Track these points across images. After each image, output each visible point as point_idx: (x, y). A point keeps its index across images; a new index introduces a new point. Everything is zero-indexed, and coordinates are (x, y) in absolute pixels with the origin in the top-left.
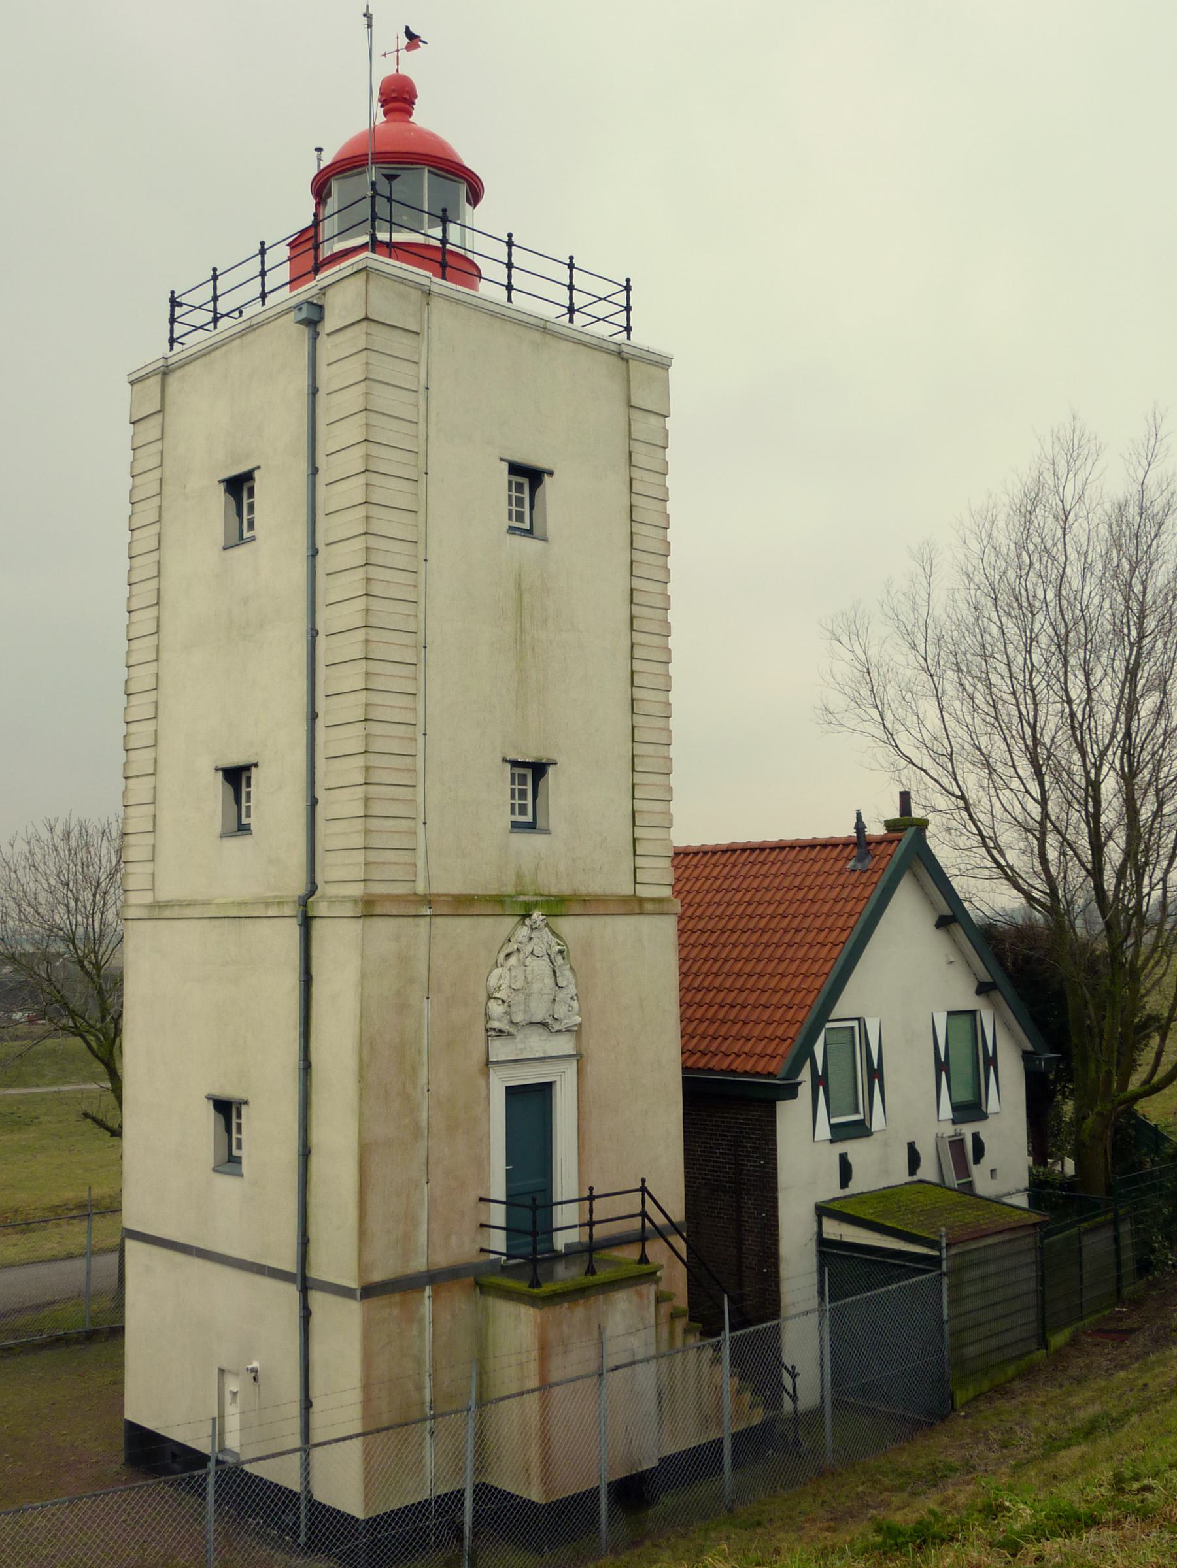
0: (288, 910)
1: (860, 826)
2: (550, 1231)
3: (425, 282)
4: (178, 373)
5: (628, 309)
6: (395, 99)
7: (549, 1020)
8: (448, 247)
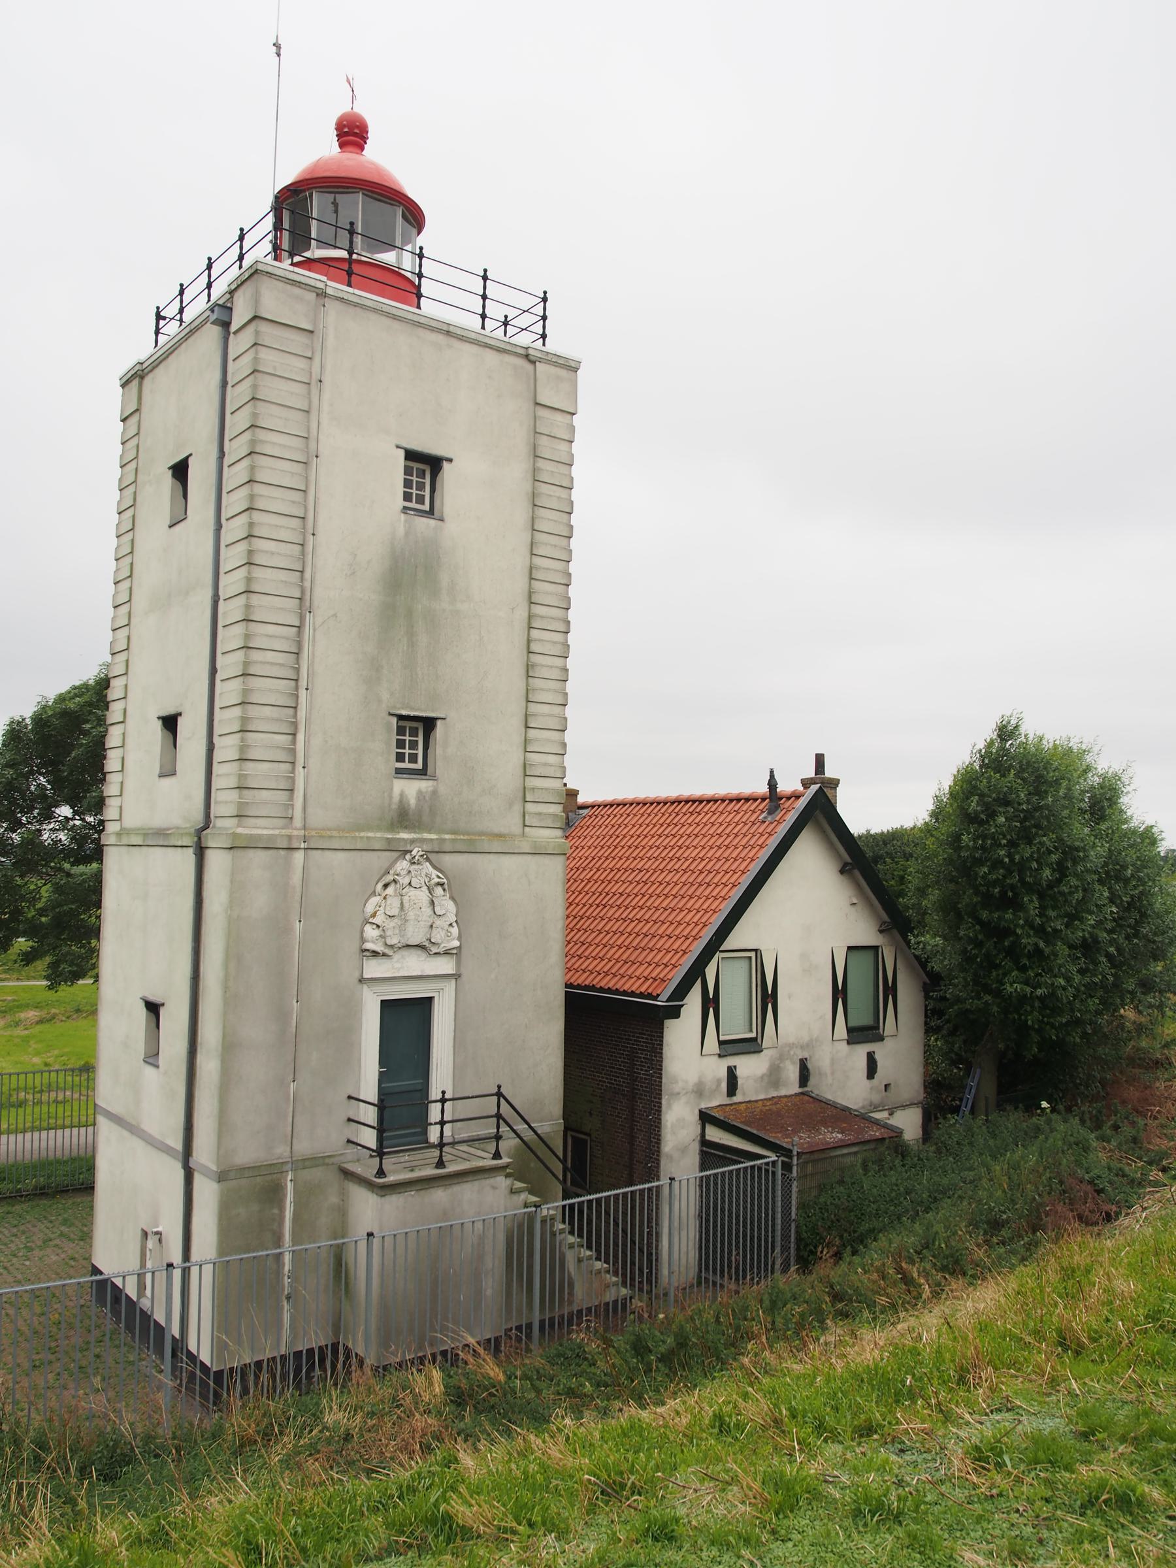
0: (188, 841)
1: (772, 784)
3: (321, 285)
4: (150, 376)
5: (544, 318)
6: (355, 135)
7: (427, 944)
8: (355, 256)
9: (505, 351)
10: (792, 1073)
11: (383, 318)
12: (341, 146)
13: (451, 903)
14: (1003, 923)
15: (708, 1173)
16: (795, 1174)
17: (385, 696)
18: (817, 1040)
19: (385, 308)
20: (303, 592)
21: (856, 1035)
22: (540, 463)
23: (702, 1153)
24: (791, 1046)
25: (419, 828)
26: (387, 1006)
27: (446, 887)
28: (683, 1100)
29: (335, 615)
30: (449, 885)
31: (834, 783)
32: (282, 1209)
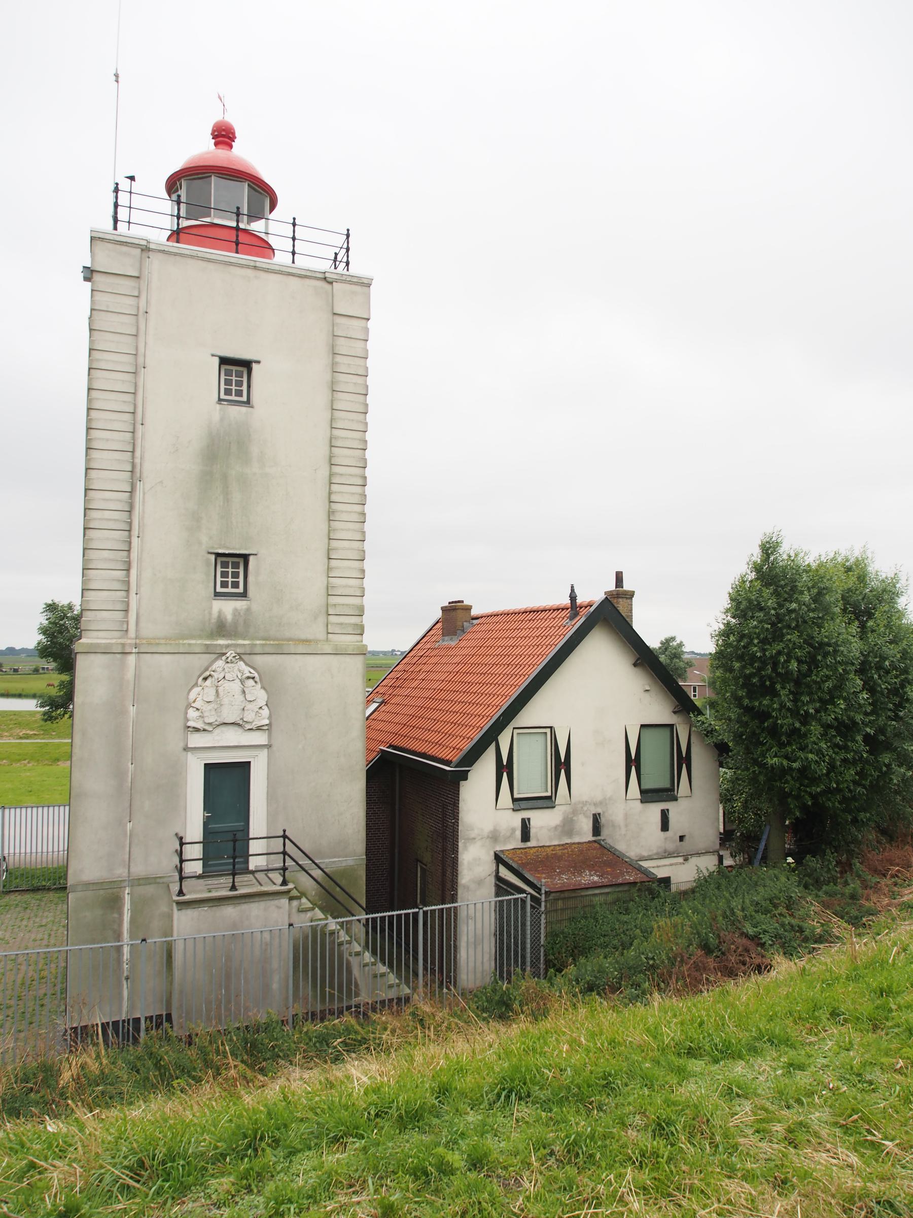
1: (573, 598)
2: (246, 856)
6: (223, 136)
9: (306, 277)
10: (586, 825)
11: (200, 262)
12: (216, 144)
13: (263, 691)
14: (762, 708)
15: (500, 899)
16: (543, 908)
17: (204, 539)
18: (610, 799)
19: (200, 254)
20: (133, 465)
21: (648, 795)
22: (338, 359)
23: (496, 885)
24: (585, 803)
25: (235, 636)
26: (209, 768)
27: (257, 679)
28: (479, 843)
29: (161, 482)
30: (265, 680)
31: (630, 595)
32: (121, 915)
